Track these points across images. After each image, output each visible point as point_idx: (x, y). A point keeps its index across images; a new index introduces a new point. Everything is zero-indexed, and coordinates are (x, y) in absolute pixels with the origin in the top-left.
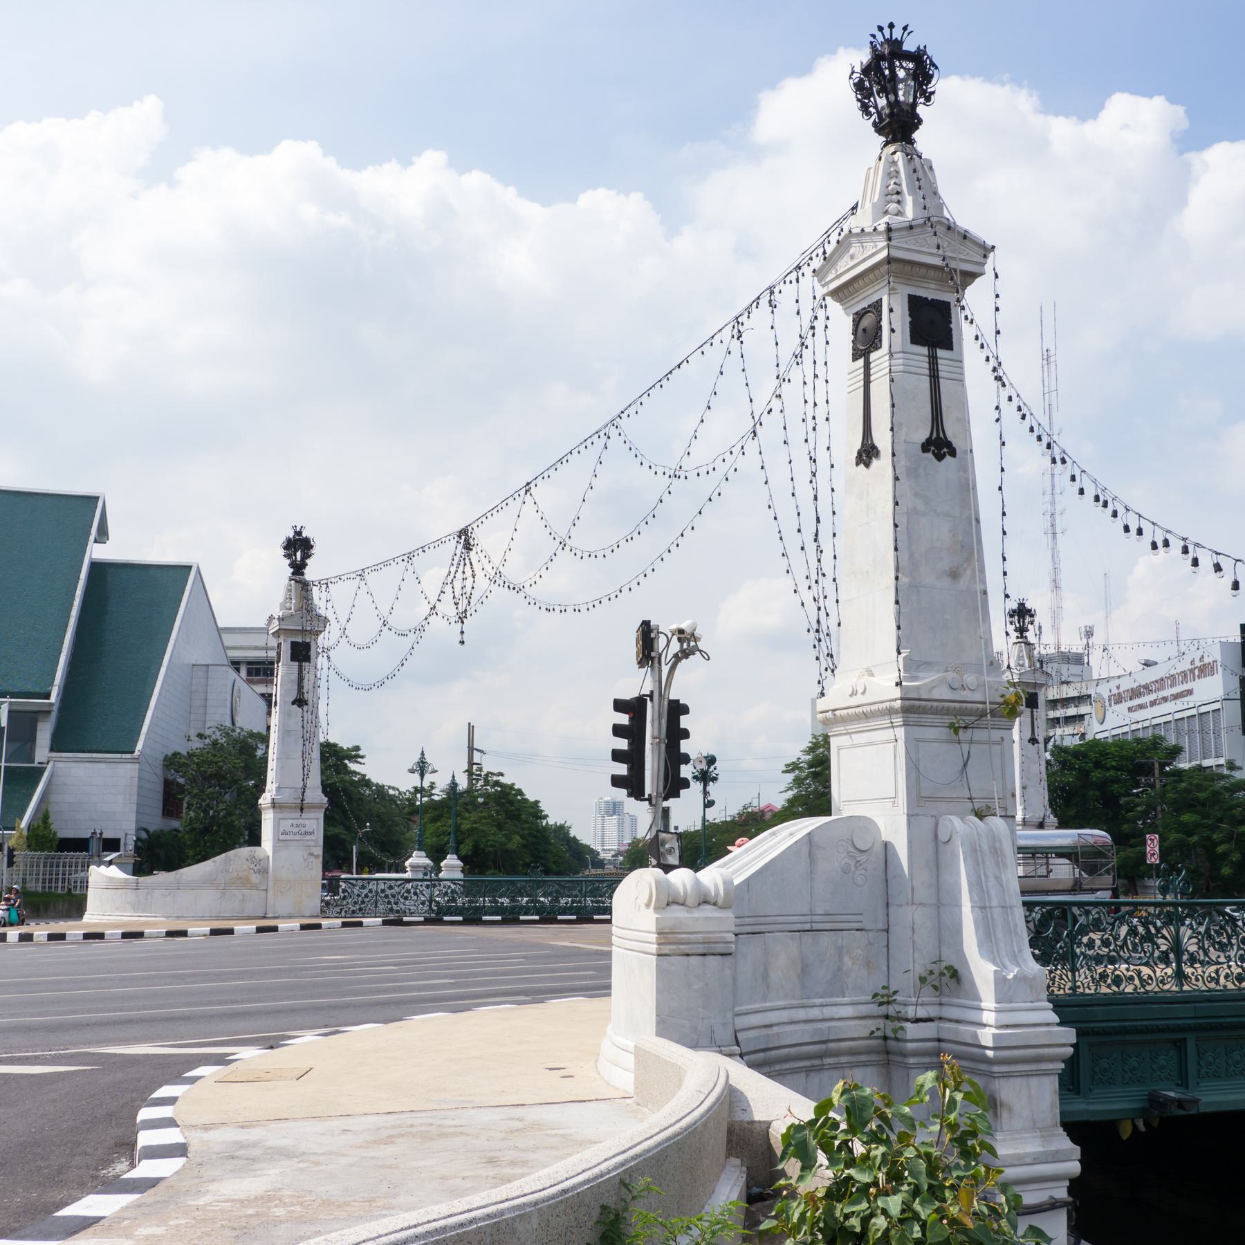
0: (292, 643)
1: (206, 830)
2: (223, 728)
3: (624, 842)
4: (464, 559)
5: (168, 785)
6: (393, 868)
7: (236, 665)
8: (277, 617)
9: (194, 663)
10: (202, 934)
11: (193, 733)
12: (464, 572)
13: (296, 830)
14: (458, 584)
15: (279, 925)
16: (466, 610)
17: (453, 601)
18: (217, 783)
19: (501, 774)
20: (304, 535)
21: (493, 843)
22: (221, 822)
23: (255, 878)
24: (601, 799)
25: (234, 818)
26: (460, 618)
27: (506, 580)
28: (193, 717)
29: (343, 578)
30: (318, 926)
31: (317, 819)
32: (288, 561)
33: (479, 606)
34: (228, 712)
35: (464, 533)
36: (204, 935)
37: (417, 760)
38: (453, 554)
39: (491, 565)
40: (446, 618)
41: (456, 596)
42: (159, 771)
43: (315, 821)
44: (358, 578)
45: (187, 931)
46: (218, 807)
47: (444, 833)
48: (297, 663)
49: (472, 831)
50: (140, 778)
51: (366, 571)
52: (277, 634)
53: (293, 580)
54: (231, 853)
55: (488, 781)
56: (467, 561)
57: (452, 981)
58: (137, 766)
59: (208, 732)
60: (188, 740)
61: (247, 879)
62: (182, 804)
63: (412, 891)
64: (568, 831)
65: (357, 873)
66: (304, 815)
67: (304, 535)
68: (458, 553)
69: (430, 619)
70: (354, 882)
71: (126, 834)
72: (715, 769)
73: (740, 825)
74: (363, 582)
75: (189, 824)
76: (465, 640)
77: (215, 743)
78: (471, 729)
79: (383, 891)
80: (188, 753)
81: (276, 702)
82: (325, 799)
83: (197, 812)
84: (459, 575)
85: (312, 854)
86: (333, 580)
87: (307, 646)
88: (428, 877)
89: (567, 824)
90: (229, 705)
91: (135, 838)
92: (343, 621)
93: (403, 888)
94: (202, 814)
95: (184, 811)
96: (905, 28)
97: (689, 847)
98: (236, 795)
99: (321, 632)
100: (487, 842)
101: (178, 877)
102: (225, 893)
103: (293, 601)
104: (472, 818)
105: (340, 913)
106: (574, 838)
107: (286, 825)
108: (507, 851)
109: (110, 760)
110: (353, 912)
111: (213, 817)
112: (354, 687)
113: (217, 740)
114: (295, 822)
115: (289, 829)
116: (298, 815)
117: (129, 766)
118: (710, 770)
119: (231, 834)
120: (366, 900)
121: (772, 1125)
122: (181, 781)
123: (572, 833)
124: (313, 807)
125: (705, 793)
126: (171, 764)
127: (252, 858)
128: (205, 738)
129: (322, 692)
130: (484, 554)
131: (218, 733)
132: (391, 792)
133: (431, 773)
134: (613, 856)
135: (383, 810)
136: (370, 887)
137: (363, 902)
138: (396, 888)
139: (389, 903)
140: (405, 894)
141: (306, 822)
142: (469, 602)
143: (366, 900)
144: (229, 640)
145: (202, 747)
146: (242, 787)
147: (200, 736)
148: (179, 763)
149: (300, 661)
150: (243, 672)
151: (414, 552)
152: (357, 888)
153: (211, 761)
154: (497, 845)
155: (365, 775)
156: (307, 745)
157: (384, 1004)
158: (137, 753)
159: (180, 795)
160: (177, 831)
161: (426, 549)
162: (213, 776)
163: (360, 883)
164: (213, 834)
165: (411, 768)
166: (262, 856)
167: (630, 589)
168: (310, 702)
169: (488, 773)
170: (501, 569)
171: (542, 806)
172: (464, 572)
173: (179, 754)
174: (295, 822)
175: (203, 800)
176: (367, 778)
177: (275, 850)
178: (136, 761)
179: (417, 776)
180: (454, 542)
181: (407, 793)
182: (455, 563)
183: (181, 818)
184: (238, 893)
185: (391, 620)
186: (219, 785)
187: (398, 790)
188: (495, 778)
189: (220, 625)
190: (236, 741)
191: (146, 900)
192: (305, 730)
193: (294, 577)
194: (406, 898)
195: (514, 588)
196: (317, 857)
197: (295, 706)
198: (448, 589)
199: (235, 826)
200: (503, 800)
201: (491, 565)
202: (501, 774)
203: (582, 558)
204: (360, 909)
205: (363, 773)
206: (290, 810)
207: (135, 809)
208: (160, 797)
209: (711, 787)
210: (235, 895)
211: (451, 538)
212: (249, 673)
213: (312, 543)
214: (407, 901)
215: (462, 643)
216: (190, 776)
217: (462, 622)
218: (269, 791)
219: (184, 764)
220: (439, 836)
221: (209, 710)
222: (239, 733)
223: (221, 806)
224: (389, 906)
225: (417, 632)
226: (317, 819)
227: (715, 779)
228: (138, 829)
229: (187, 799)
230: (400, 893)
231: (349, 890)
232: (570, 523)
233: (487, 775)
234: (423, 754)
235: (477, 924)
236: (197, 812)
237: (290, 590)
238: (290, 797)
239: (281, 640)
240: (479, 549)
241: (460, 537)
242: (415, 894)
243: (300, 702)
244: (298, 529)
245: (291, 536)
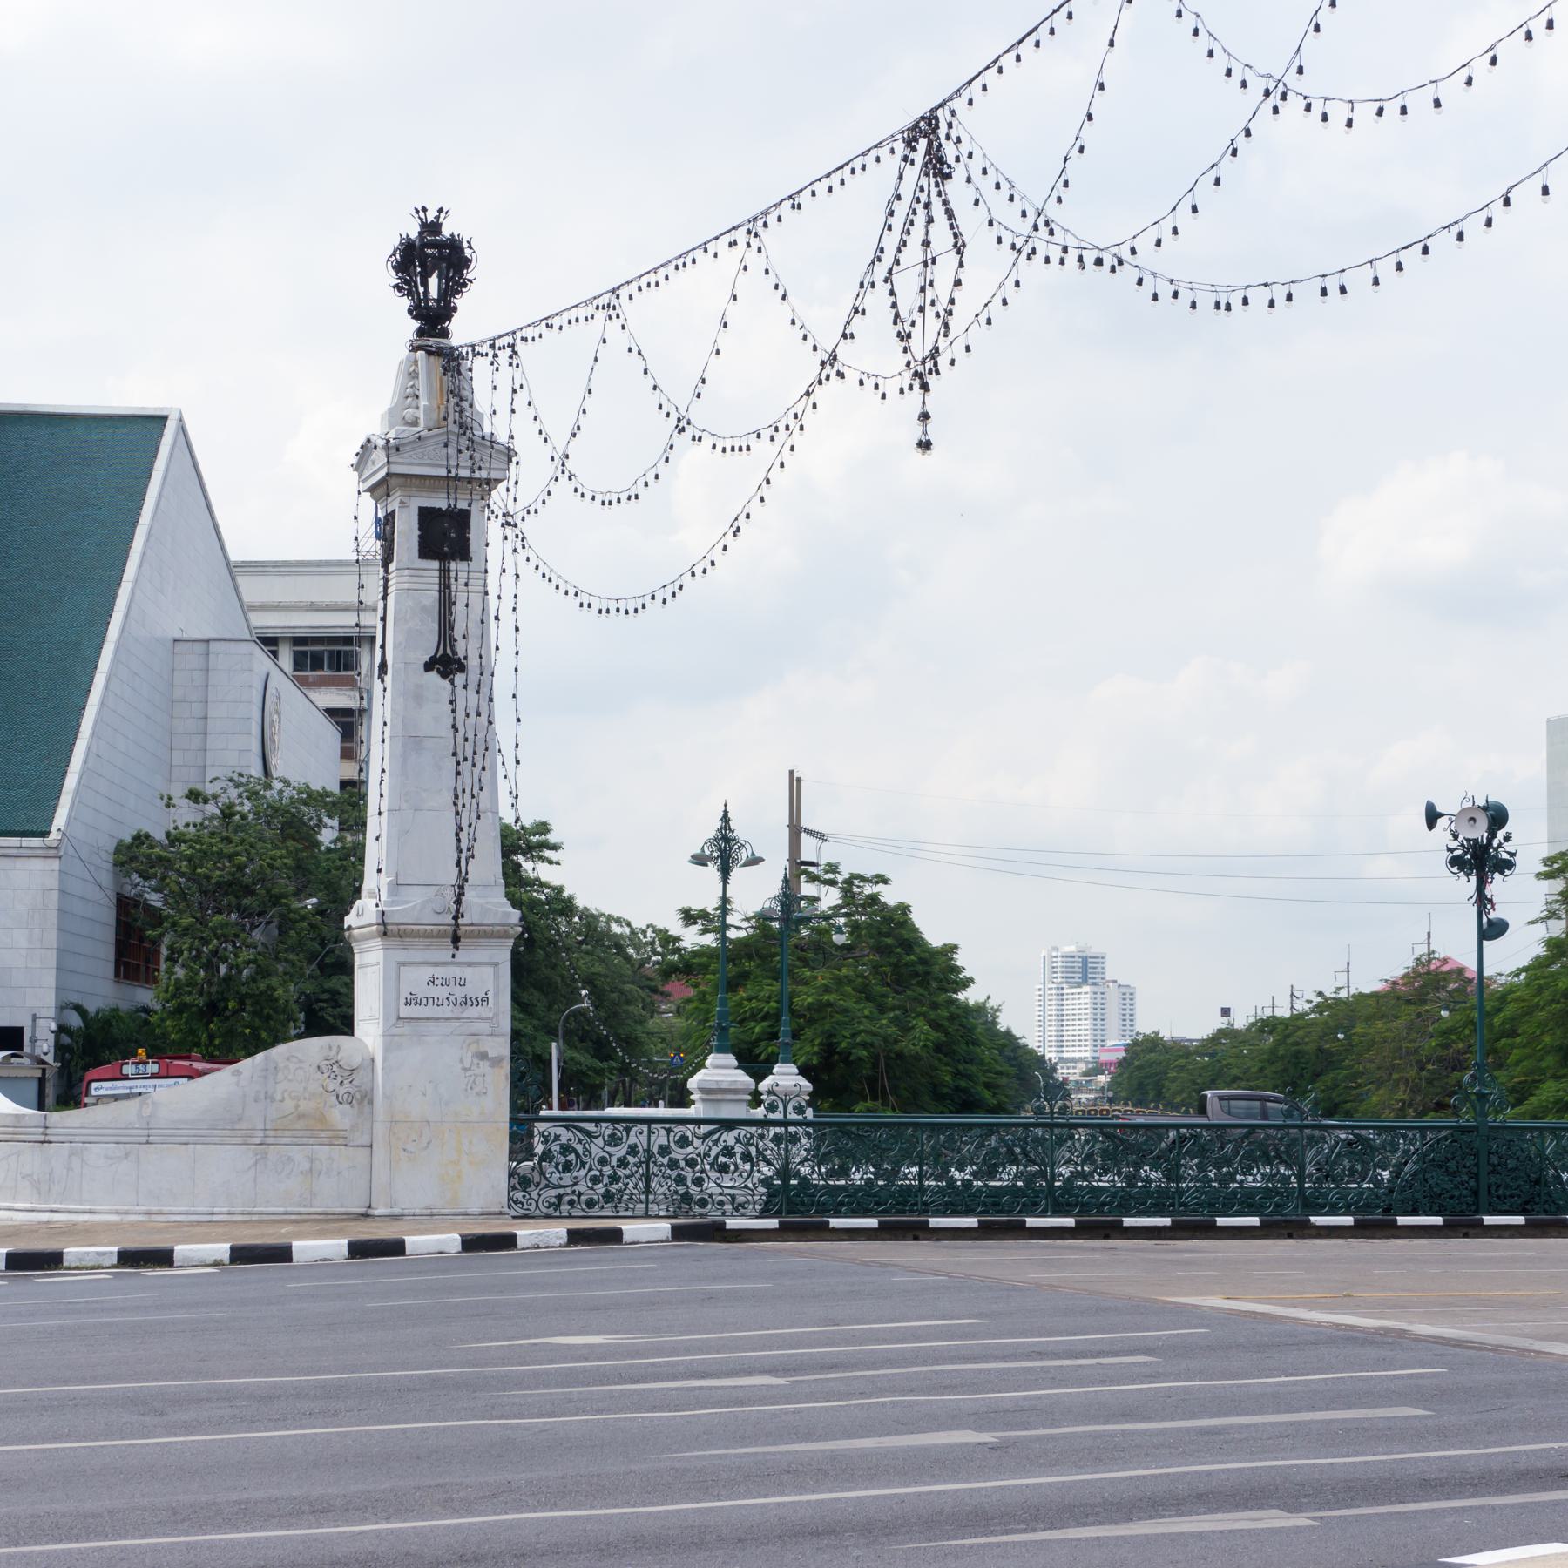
0: (420, 509)
1: (213, 1009)
2: (243, 780)
3: (1110, 1043)
4: (927, 206)
5: (126, 907)
6: (620, 1096)
7: (270, 642)
8: (381, 443)
9: (178, 635)
10: (210, 1260)
11: (178, 792)
12: (926, 243)
13: (440, 992)
14: (907, 283)
16: (936, 349)
17: (893, 330)
18: (234, 901)
19: (883, 880)
20: (446, 232)
21: (868, 1039)
22: (244, 990)
23: (340, 1116)
24: (1057, 949)
25: (275, 981)
26: (917, 374)
27: (1071, 242)
28: (177, 758)
29: (556, 322)
30: (508, 1241)
31: (496, 965)
32: (406, 302)
33: (978, 334)
34: (256, 746)
35: (926, 129)
36: (216, 1264)
37: (712, 833)
38: (889, 195)
39: (1018, 206)
40: (869, 383)
41: (903, 315)
42: (106, 876)
43: (490, 970)
44: (602, 315)
45: (172, 1251)
46: (236, 956)
47: (753, 1017)
48: (435, 564)
49: (820, 1007)
50: (63, 892)
51: (624, 293)
52: (381, 490)
53: (419, 348)
54: (280, 1050)
55: (853, 896)
56: (938, 210)
57: (986, 1437)
58: (55, 865)
59: (210, 789)
60: (168, 806)
61: (322, 1119)
62: (158, 952)
63: (739, 1149)
64: (995, 1018)
65: (562, 1107)
66: (462, 955)
67: (446, 232)
68: (907, 191)
69: (819, 394)
70: (590, 1127)
71: (34, 1018)
72: (1507, 838)
73: (1409, 1002)
74: (616, 323)
75: (174, 997)
76: (931, 436)
77: (227, 813)
78: (795, 783)
79: (664, 1150)
80: (168, 834)
81: (383, 667)
82: (515, 915)
83: (191, 969)
84: (913, 253)
85: (483, 1056)
86: (528, 333)
87: (461, 520)
88: (778, 1116)
89: (991, 1004)
90: (256, 730)
91: (54, 1026)
92: (560, 438)
93: (716, 1143)
94: (202, 973)
95: (163, 967)
96: (440, 211)
97: (1281, 1052)
98: (276, 932)
99: (499, 481)
100: (853, 1035)
101: (147, 1111)
102: (265, 1156)
103: (423, 403)
104: (820, 981)
105: (557, 1206)
106: (1008, 1033)
107: (416, 979)
108: (900, 1055)
110: (591, 1204)
111: (228, 979)
112: (595, 608)
113: (231, 806)
114: (440, 972)
115: (423, 991)
116: (445, 953)
117: (37, 865)
118: (1495, 843)
119: (268, 1018)
120: (620, 1172)
122: (155, 899)
123: (1004, 1023)
124: (486, 934)
125: (1483, 901)
126: (132, 859)
127: (333, 1066)
128: (206, 801)
129: (500, 633)
130: (992, 177)
131: (233, 793)
132: (616, 929)
133: (745, 865)
134: (1085, 1074)
135: (599, 968)
136: (632, 1140)
137: (614, 1179)
138: (697, 1143)
139: (681, 1180)
140: (722, 1159)
141: (468, 973)
142: (946, 326)
143: (620, 1172)
144: (253, 589)
145: (199, 820)
146: (290, 911)
147: (195, 796)
148: (148, 857)
149: (443, 558)
150: (286, 657)
151: (765, 213)
152: (600, 1141)
153: (220, 854)
154: (877, 1041)
155: (559, 890)
156: (467, 774)
157: (816, 1534)
158: (54, 835)
159: (153, 928)
160: (146, 1010)
161: (805, 198)
162: (226, 887)
163: (606, 1129)
164: (227, 1018)
165: (698, 851)
166: (356, 1061)
167: (1545, 191)
168: (473, 663)
169: (853, 877)
170: (1052, 210)
171: (960, 959)
172: (926, 243)
173: (147, 836)
174: (440, 972)
175: (206, 942)
176: (565, 894)
177: (391, 1041)
178: (52, 852)
179: (712, 872)
180: (892, 163)
181: (650, 933)
182: (898, 222)
183: (156, 981)
184: (298, 1154)
185: (700, 415)
186: (239, 908)
187: (629, 924)
188: (869, 889)
189: (234, 556)
190: (275, 809)
191: (69, 1169)
192: (460, 735)
193: (423, 342)
194: (723, 1169)
195: (1099, 262)
196: (496, 1062)
197: (433, 675)
198: (877, 301)
199: (277, 1000)
200: (889, 941)
201: (1018, 206)
202: (883, 880)
203: (1350, 123)
204: (608, 1197)
205: (556, 883)
206: (427, 942)
207: (54, 963)
208: (110, 935)
209: (1498, 887)
210: (290, 1159)
211: (884, 152)
212: (299, 664)
213: (468, 252)
214: (727, 1177)
215: (925, 445)
216: (175, 888)
217: (925, 387)
218: (372, 895)
219: (160, 858)
220: (741, 1022)
221: (212, 742)
222: (281, 792)
223: (246, 955)
224: (681, 1190)
225: (781, 436)
226: (496, 965)
227: (1505, 866)
228: (62, 1007)
229: (167, 940)
230: (707, 1155)
231: (579, 1148)
232: (1304, 22)
233: (849, 882)
234: (725, 818)
235: (916, 1238)
236: (191, 969)
237: (413, 375)
238: (422, 907)
239: (394, 504)
240: (975, 167)
241: (910, 143)
242: (746, 1157)
243: (446, 663)
244: (431, 217)
245: (414, 235)
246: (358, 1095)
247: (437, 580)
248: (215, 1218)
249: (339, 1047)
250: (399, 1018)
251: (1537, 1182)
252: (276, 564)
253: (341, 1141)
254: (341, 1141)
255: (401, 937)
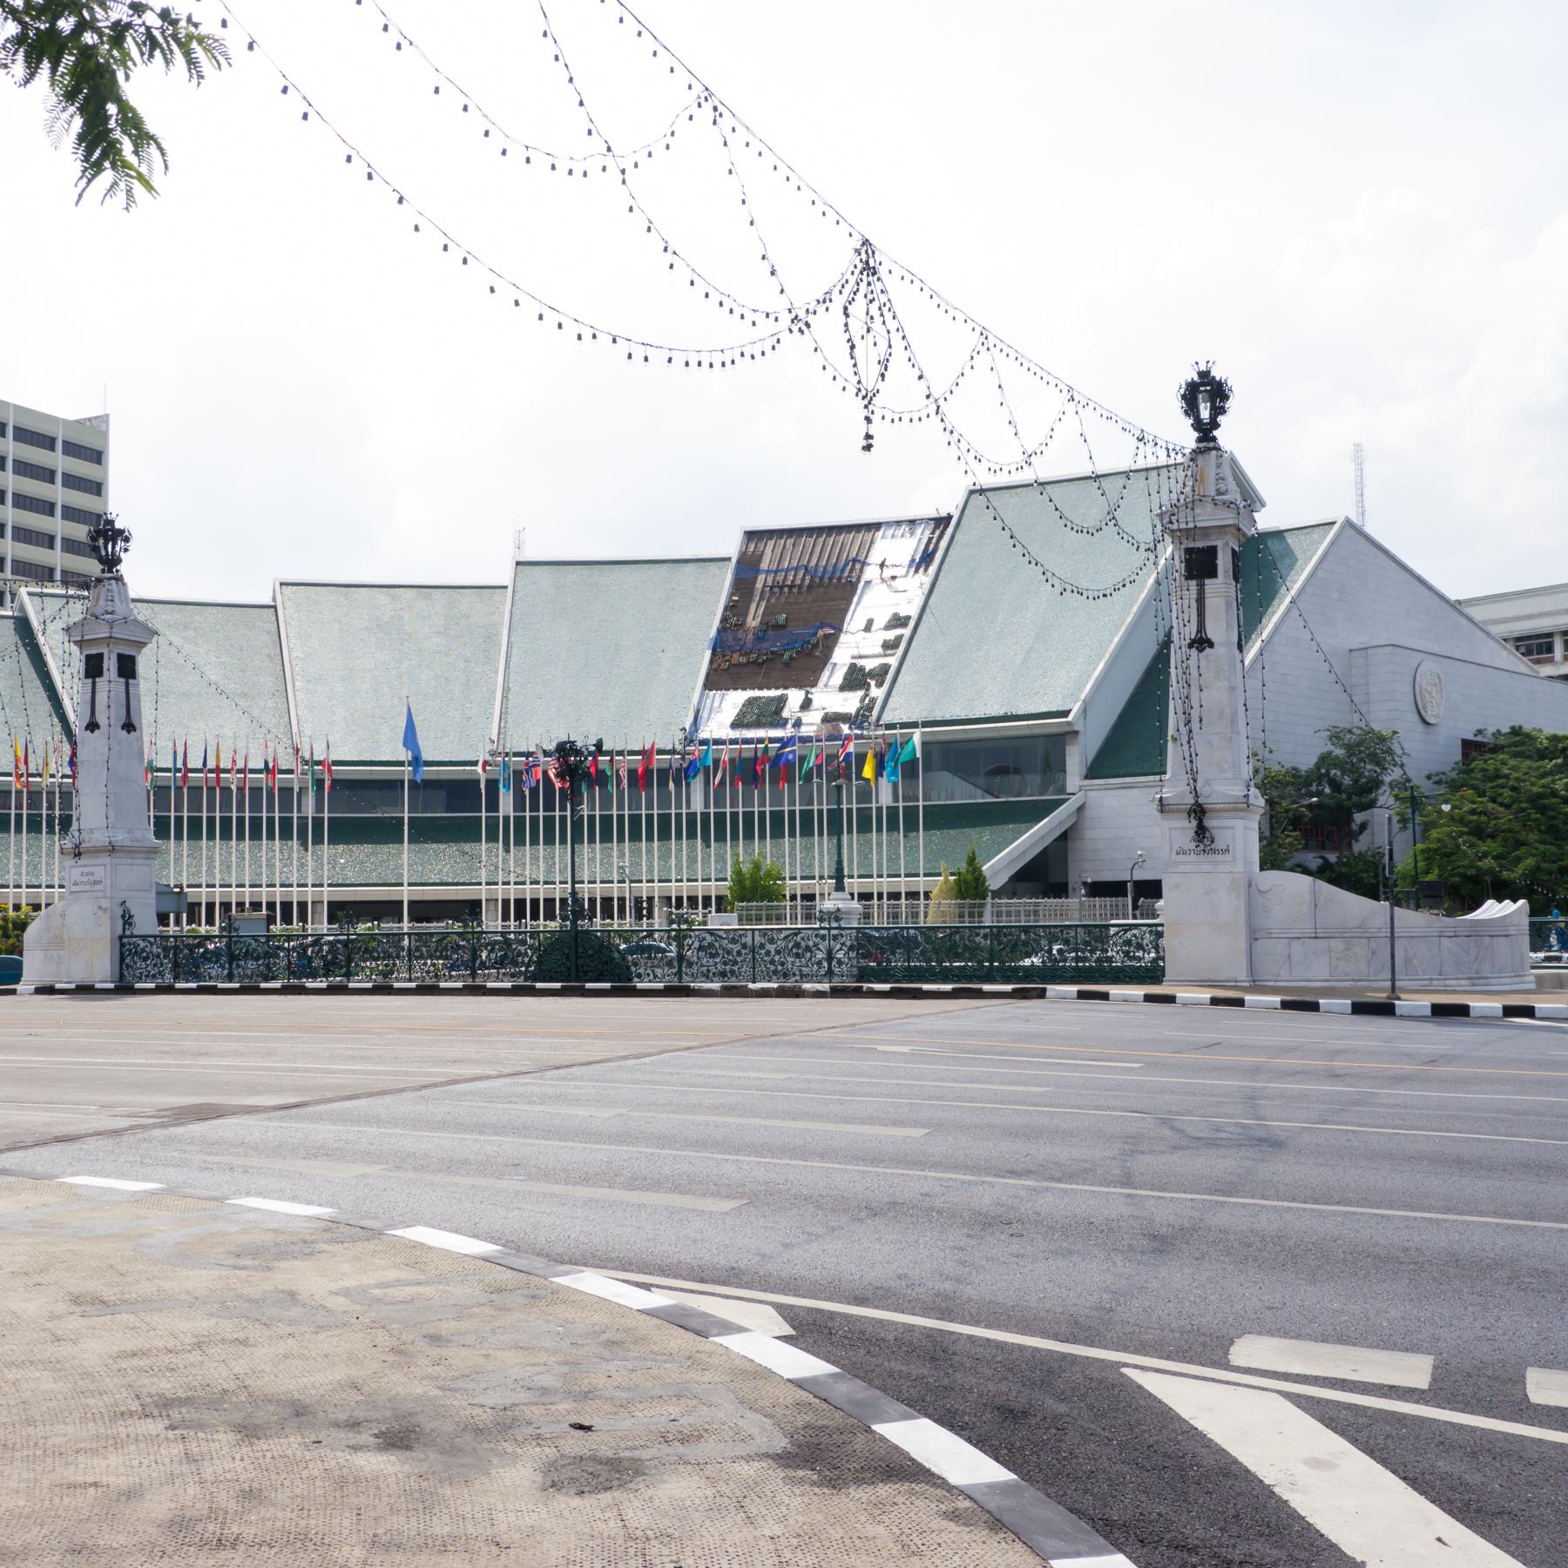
13: (85, 879)
15: (1178, 995)
31: (105, 865)
109: (1144, 785)
115: (80, 879)
120: (739, 959)
121: (781, 1443)
139: (772, 962)
143: (739, 959)
170: (941, 402)
226: (105, 865)
248: (1238, 984)
251: (606, 963)
252: (1546, 589)
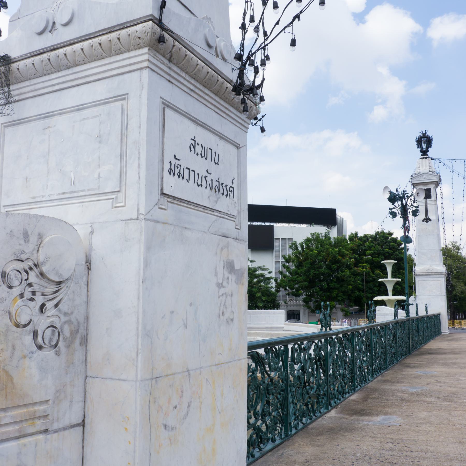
96: (426, 131)
246: (67, 331)
247: (428, 203)
249: (40, 236)
250: (163, 194)
253: (40, 425)
254: (40, 425)
255: (170, 60)
